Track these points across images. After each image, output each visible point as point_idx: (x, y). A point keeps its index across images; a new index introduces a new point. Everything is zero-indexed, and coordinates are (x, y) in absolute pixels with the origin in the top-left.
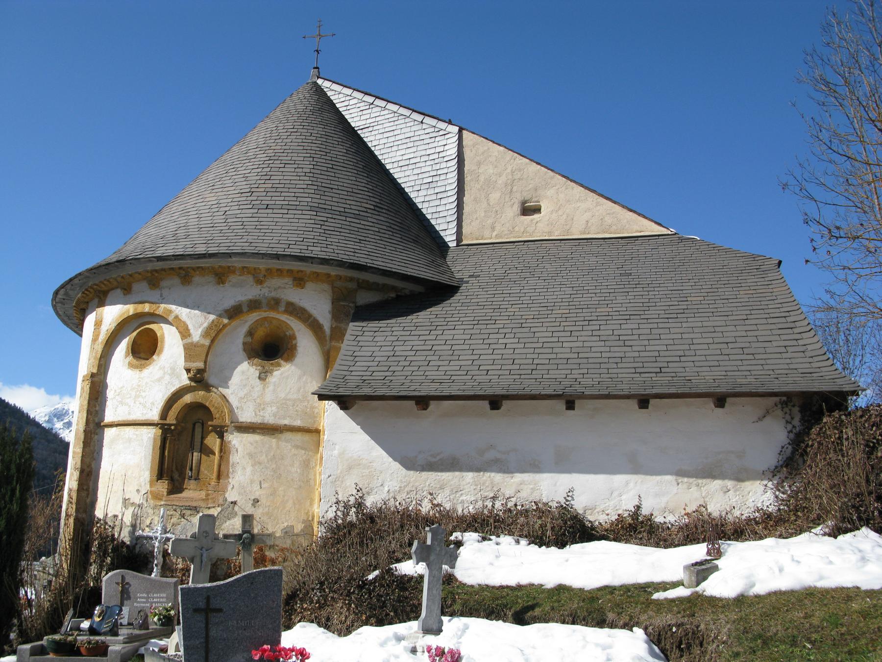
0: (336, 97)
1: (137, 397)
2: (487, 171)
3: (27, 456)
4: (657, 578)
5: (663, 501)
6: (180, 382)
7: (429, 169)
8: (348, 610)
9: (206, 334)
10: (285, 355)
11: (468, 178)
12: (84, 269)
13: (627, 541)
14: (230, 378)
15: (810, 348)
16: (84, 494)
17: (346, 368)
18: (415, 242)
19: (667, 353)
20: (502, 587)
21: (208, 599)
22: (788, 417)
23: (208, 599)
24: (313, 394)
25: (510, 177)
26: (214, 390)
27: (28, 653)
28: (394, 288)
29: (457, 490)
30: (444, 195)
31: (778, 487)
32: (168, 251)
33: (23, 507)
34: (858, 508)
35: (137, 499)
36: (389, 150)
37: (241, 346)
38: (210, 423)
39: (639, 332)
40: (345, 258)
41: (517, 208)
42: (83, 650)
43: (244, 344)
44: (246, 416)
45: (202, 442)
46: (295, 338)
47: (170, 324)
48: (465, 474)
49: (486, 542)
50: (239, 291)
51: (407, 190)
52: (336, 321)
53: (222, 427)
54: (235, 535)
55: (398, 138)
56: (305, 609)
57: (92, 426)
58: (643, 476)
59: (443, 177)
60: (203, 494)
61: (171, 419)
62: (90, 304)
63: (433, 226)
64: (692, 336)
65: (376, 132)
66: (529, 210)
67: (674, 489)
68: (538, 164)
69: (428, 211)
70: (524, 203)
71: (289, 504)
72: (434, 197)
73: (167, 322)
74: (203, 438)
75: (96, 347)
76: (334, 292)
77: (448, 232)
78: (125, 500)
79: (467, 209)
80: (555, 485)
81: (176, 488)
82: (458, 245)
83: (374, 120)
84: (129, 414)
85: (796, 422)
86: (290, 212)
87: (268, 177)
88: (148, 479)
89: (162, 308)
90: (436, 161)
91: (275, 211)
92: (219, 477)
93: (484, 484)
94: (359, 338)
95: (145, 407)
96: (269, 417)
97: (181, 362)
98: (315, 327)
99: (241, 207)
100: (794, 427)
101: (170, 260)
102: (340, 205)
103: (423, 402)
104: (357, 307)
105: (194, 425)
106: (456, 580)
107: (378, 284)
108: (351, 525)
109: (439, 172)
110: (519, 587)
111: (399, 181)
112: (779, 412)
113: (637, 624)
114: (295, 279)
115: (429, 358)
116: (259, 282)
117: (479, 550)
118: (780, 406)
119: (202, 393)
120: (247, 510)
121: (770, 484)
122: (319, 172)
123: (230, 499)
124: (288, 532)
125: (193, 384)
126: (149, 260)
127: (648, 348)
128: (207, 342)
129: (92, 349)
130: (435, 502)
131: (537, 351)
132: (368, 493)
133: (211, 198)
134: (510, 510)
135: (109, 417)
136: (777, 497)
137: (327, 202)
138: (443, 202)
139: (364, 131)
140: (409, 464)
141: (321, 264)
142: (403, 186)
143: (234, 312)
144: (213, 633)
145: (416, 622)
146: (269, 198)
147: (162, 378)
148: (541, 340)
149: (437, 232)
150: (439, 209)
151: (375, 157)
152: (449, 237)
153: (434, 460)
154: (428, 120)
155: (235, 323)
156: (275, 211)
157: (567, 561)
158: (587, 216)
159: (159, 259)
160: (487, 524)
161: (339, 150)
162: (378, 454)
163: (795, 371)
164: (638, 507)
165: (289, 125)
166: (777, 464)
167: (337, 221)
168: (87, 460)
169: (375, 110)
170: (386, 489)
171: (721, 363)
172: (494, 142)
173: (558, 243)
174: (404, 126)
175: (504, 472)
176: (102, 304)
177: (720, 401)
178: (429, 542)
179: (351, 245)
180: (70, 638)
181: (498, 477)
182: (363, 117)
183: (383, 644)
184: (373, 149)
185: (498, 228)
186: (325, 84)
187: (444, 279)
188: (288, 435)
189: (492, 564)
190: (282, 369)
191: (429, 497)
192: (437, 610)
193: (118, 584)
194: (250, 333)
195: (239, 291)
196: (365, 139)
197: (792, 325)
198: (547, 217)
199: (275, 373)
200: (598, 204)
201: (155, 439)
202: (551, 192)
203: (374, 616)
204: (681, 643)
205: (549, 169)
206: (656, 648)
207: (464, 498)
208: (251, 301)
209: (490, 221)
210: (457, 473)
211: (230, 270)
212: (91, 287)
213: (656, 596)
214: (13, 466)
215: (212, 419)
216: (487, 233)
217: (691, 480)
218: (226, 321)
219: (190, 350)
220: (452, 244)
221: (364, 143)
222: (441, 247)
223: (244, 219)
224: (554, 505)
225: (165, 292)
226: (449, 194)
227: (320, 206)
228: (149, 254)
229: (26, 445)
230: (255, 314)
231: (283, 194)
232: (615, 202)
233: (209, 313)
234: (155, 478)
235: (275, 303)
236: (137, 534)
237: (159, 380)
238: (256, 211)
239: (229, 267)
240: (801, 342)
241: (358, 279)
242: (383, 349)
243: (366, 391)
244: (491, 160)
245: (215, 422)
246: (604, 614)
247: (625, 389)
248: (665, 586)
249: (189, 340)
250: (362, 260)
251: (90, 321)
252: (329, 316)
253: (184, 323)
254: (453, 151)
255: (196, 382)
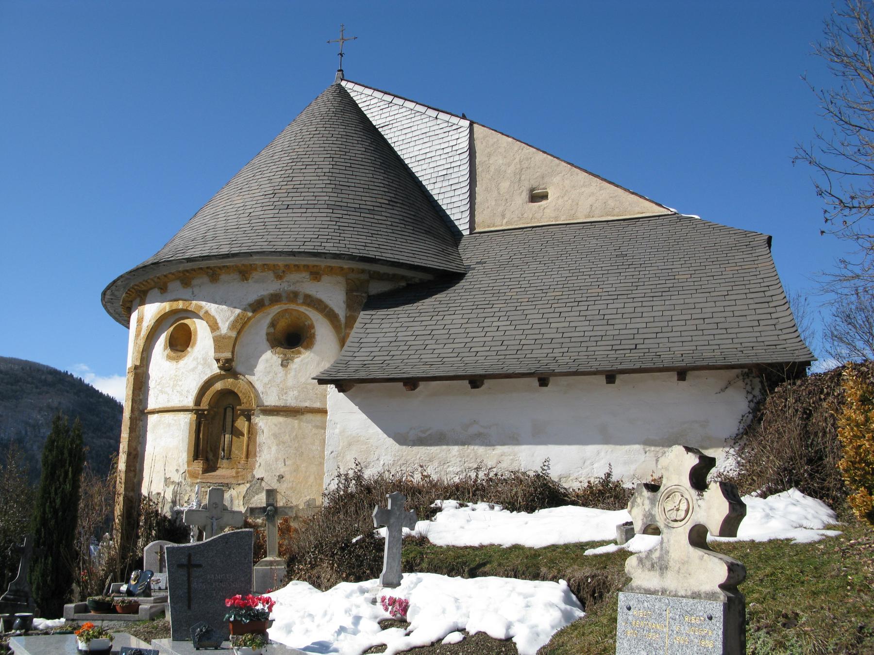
0: (359, 97)
1: (174, 386)
2: (498, 161)
3: (78, 442)
4: (584, 539)
5: (631, 469)
6: (212, 371)
7: (444, 162)
8: (332, 568)
9: (232, 327)
10: (305, 343)
11: (479, 170)
12: (125, 272)
13: (595, 506)
14: (255, 366)
15: (781, 320)
16: (131, 474)
17: (351, 354)
18: (427, 232)
19: (645, 331)
20: (466, 547)
21: (189, 556)
22: (749, 388)
23: (189, 556)
24: (314, 379)
25: (518, 166)
26: (241, 377)
27: (73, 611)
28: (403, 278)
29: (444, 462)
30: (458, 186)
31: (740, 453)
32: (196, 253)
33: (76, 486)
34: (791, 471)
35: (177, 478)
36: (407, 146)
37: (264, 337)
38: (238, 407)
39: (623, 311)
40: (356, 252)
41: (525, 196)
42: (118, 608)
43: (268, 334)
44: (271, 400)
45: (233, 425)
46: (313, 328)
47: (202, 319)
48: (451, 447)
49: (463, 509)
50: (261, 287)
51: (424, 183)
52: (350, 310)
53: (249, 411)
54: (260, 508)
55: (415, 134)
56: (301, 570)
57: (136, 413)
58: (612, 446)
59: (456, 169)
60: (233, 472)
61: (204, 405)
62: (134, 303)
63: (448, 216)
64: (672, 313)
65: (395, 129)
66: (536, 197)
67: (642, 457)
68: (544, 152)
69: (443, 202)
70: (532, 190)
71: (311, 480)
72: (449, 188)
73: (199, 317)
74: (233, 421)
75: (139, 341)
76: (347, 284)
77: (462, 221)
78: (166, 479)
79: (479, 199)
80: (533, 455)
81: (210, 467)
82: (471, 233)
83: (393, 118)
84: (168, 401)
85: (757, 392)
86: (309, 211)
87: (290, 179)
88: (186, 460)
89: (194, 305)
90: (450, 154)
91: (295, 211)
92: (247, 457)
93: (468, 456)
94: (367, 326)
95: (181, 395)
96: (291, 400)
97: (212, 353)
98: (331, 316)
99: (265, 208)
100: (754, 396)
101: (198, 261)
102: (356, 201)
103: (411, 383)
104: (369, 296)
105: (225, 409)
106: (429, 542)
107: (388, 275)
108: (352, 496)
109: (453, 165)
110: (482, 547)
111: (417, 175)
112: (740, 383)
113: (563, 577)
114: (312, 273)
115: (426, 342)
116: (279, 277)
117: (453, 515)
118: (741, 377)
119: (231, 380)
120: (273, 485)
121: (732, 451)
122: (338, 171)
123: (257, 476)
124: (309, 504)
125: (223, 372)
126: (180, 261)
127: (629, 326)
128: (234, 334)
129: (136, 343)
130: (425, 474)
131: (526, 332)
132: (366, 467)
133: (238, 201)
134: (491, 479)
135: (152, 405)
136: (738, 463)
137: (344, 200)
138: (457, 192)
139: (384, 128)
140: (402, 439)
141: (334, 258)
142: (420, 179)
143: (257, 306)
144: (194, 585)
145: (378, 580)
146: (290, 199)
147: (196, 368)
148: (531, 322)
149: (452, 222)
150: (454, 200)
151: (395, 152)
152: (463, 226)
153: (423, 435)
154: (442, 116)
155: (259, 315)
156: (295, 211)
157: (526, 523)
158: (591, 200)
159: (189, 260)
160: (467, 493)
161: (358, 149)
162: (374, 431)
163: (762, 344)
164: (609, 475)
165: (312, 128)
166: (737, 432)
167: (351, 217)
168: (134, 444)
169: (394, 108)
170: (382, 463)
171: (694, 338)
172: (503, 134)
173: (563, 228)
174: (420, 122)
175: (487, 445)
176: (143, 303)
177: (682, 374)
178: (389, 507)
179: (363, 239)
180: (108, 599)
181: (481, 450)
182: (383, 116)
183: (348, 596)
184: (393, 145)
185: (508, 215)
186: (348, 86)
187: (451, 267)
188: (309, 417)
189: (462, 528)
190: (302, 356)
191: (420, 469)
192: (397, 566)
193: (157, 553)
194: (273, 324)
195: (261, 287)
196: (385, 137)
197: (769, 299)
198: (554, 203)
199: (296, 360)
200: (601, 189)
201: (191, 424)
202: (557, 179)
203: (353, 574)
204: (594, 592)
205: (554, 157)
206: (574, 597)
207: (451, 469)
208: (272, 295)
209: (500, 209)
210: (444, 447)
211: (253, 268)
212: (133, 288)
213: (587, 553)
214: (66, 452)
215: (240, 404)
216: (498, 221)
217: (658, 449)
218: (250, 314)
219: (219, 342)
220: (466, 233)
221: (385, 141)
222: (456, 235)
223: (266, 220)
224: (532, 474)
225: (196, 290)
226: (463, 185)
227: (337, 203)
228: (180, 256)
229: (77, 432)
230: (276, 307)
231: (303, 194)
232: (617, 186)
233: (235, 308)
234: (192, 458)
235: (293, 296)
236: (175, 509)
237: (193, 370)
238: (277, 211)
239: (251, 265)
240: (774, 316)
241: (369, 271)
242: (387, 335)
243: (362, 375)
244: (501, 152)
245: (243, 407)
246: (539, 568)
247: (595, 365)
248: (594, 544)
249: (217, 333)
250: (371, 253)
251: (134, 317)
252: (343, 306)
253: (213, 317)
254: (464, 144)
255: (225, 370)
